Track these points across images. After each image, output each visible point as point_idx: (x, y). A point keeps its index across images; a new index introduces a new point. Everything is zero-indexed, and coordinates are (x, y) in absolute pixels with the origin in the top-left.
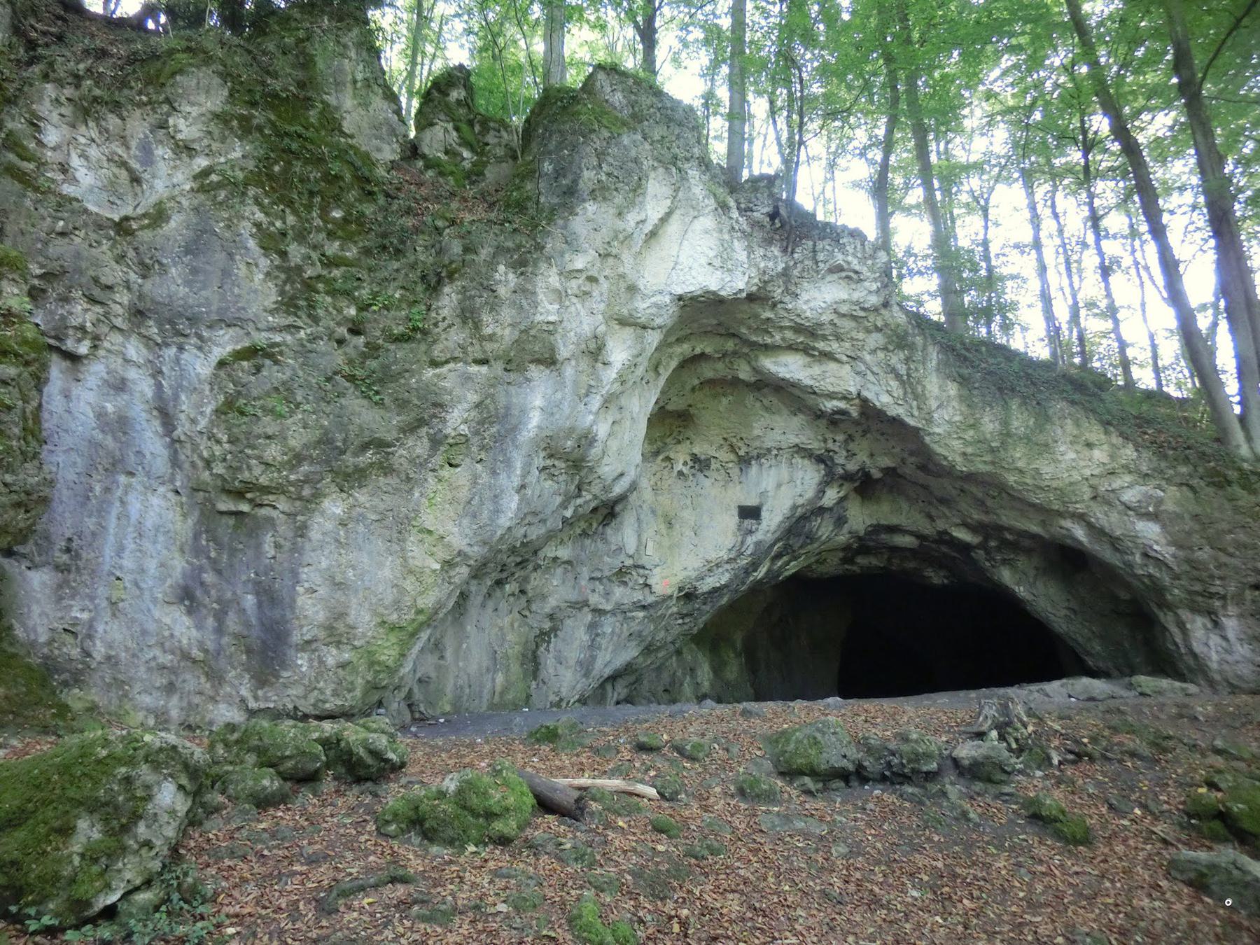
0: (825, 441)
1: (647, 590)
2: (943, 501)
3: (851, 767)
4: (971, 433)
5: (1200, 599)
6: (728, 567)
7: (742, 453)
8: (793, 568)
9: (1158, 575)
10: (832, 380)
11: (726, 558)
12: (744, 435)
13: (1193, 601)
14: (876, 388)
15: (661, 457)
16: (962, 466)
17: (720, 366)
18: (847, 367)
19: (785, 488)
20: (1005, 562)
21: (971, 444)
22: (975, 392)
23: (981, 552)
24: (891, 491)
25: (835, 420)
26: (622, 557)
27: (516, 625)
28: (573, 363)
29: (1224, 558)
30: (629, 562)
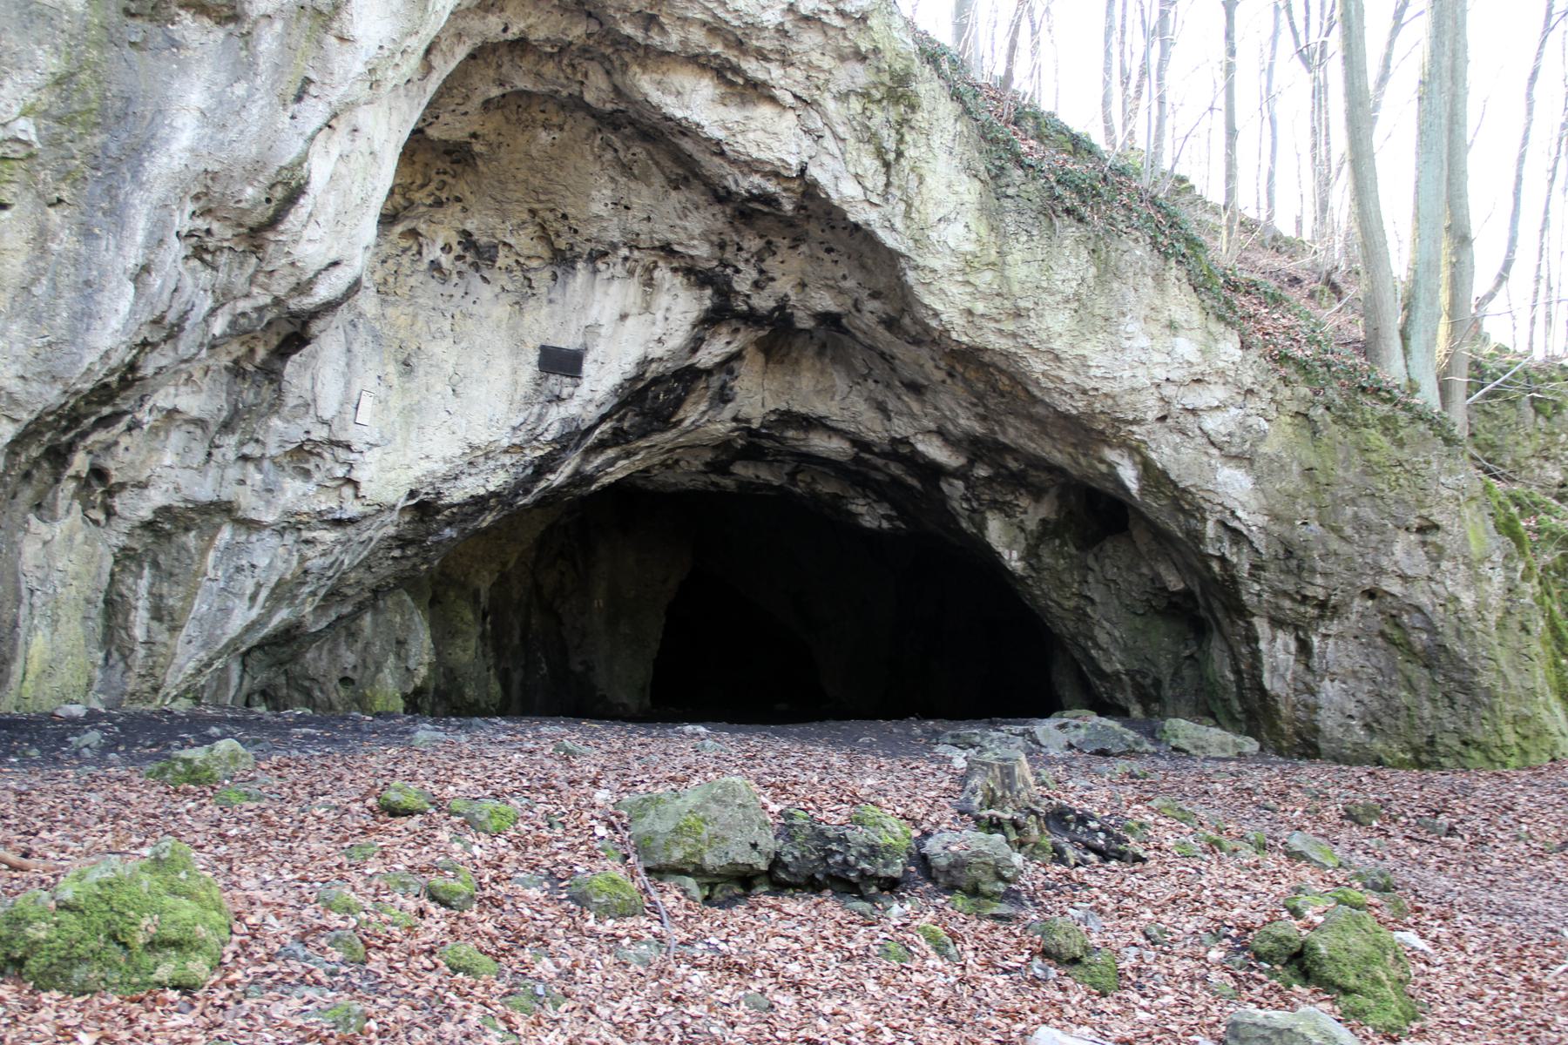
0: (722, 246)
1: (348, 491)
2: (915, 388)
3: (763, 865)
4: (988, 276)
5: (1287, 604)
6: (507, 460)
7: (562, 244)
8: (620, 470)
9: (1235, 560)
10: (760, 136)
11: (505, 443)
12: (570, 211)
13: (1278, 608)
14: (836, 166)
15: (399, 229)
16: (961, 334)
17: (549, 69)
18: (791, 115)
19: (629, 326)
20: (996, 505)
21: (985, 297)
22: (1008, 203)
23: (960, 484)
24: (822, 350)
25: (749, 212)
26: (308, 422)
27: (79, 537)
28: (278, 26)
29: (1335, 544)
30: (320, 433)
